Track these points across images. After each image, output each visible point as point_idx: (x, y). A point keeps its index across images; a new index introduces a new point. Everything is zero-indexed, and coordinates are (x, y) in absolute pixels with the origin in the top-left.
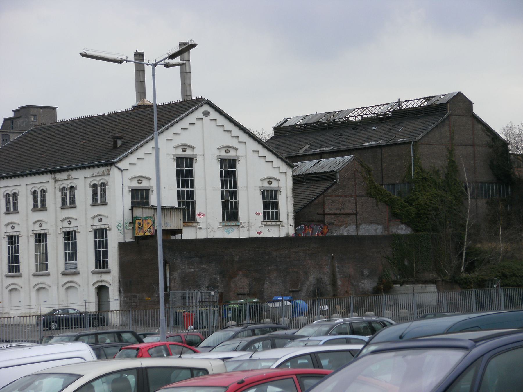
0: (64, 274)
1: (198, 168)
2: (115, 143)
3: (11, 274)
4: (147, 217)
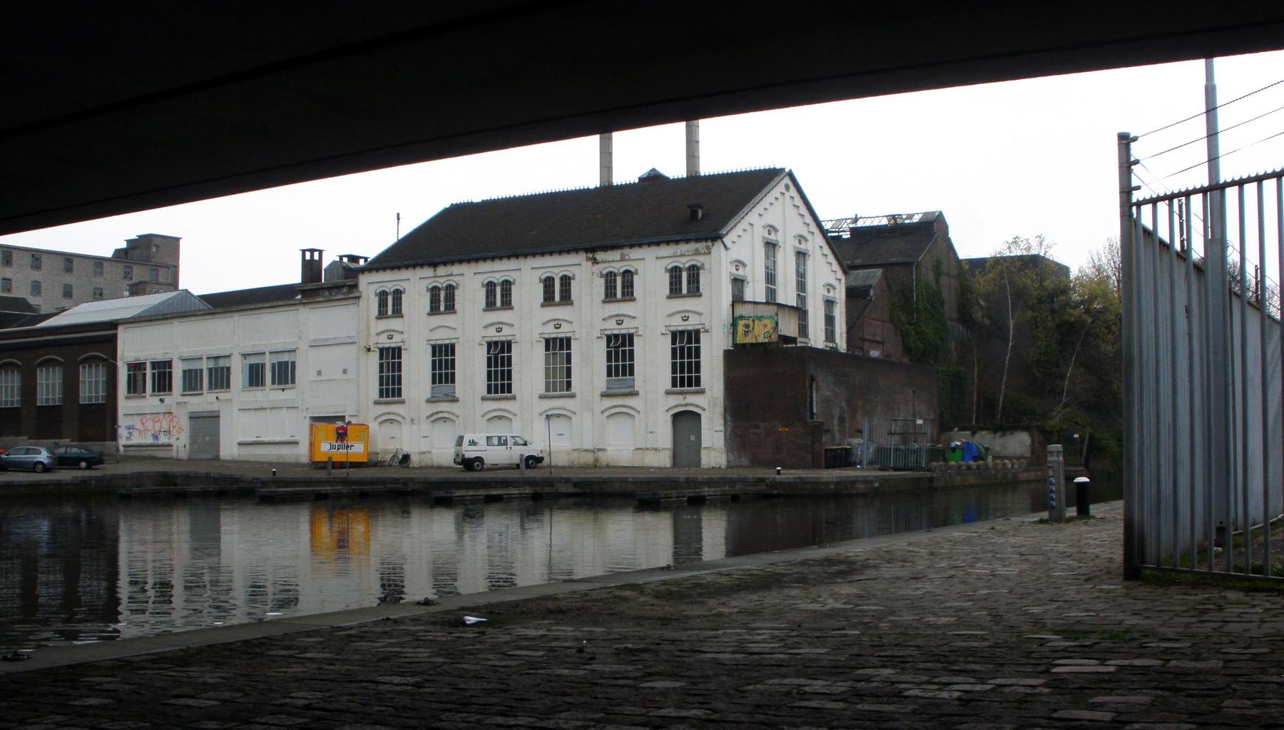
0: (604, 395)
1: (780, 255)
2: (694, 214)
3: (385, 399)
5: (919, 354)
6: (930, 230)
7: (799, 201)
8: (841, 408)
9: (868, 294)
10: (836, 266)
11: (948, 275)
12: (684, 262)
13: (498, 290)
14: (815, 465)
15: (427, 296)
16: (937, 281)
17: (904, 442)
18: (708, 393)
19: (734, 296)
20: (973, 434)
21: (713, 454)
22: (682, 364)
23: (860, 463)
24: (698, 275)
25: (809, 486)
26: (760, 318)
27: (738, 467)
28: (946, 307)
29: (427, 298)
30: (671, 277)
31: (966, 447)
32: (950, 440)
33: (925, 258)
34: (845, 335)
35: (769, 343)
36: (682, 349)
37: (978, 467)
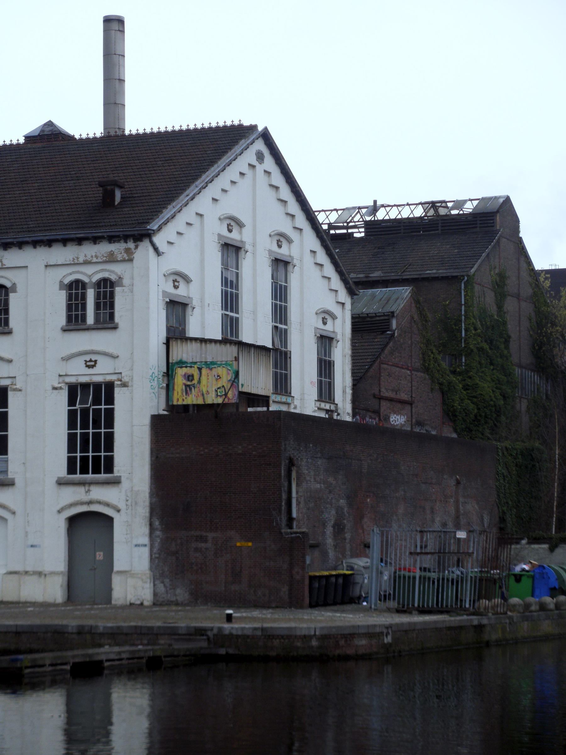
1: (246, 265)
2: (108, 197)
4: (213, 363)
5: (471, 421)
6: (492, 223)
7: (278, 179)
8: (339, 510)
9: (388, 328)
10: (336, 283)
11: (518, 296)
12: (91, 274)
13: (91, 295)
14: (294, 603)
15: (62, 298)
16: (500, 307)
17: (441, 566)
18: (125, 484)
19: (169, 329)
20: (552, 549)
21: (131, 582)
22: (85, 437)
23: (366, 599)
24: (112, 295)
25: (276, 642)
26: (210, 365)
27: (169, 603)
28: (513, 346)
29: (60, 299)
30: (70, 297)
31: (539, 574)
32: (511, 563)
33: (481, 271)
34: (349, 391)
35: (223, 405)
36: (85, 412)
37: (558, 606)
